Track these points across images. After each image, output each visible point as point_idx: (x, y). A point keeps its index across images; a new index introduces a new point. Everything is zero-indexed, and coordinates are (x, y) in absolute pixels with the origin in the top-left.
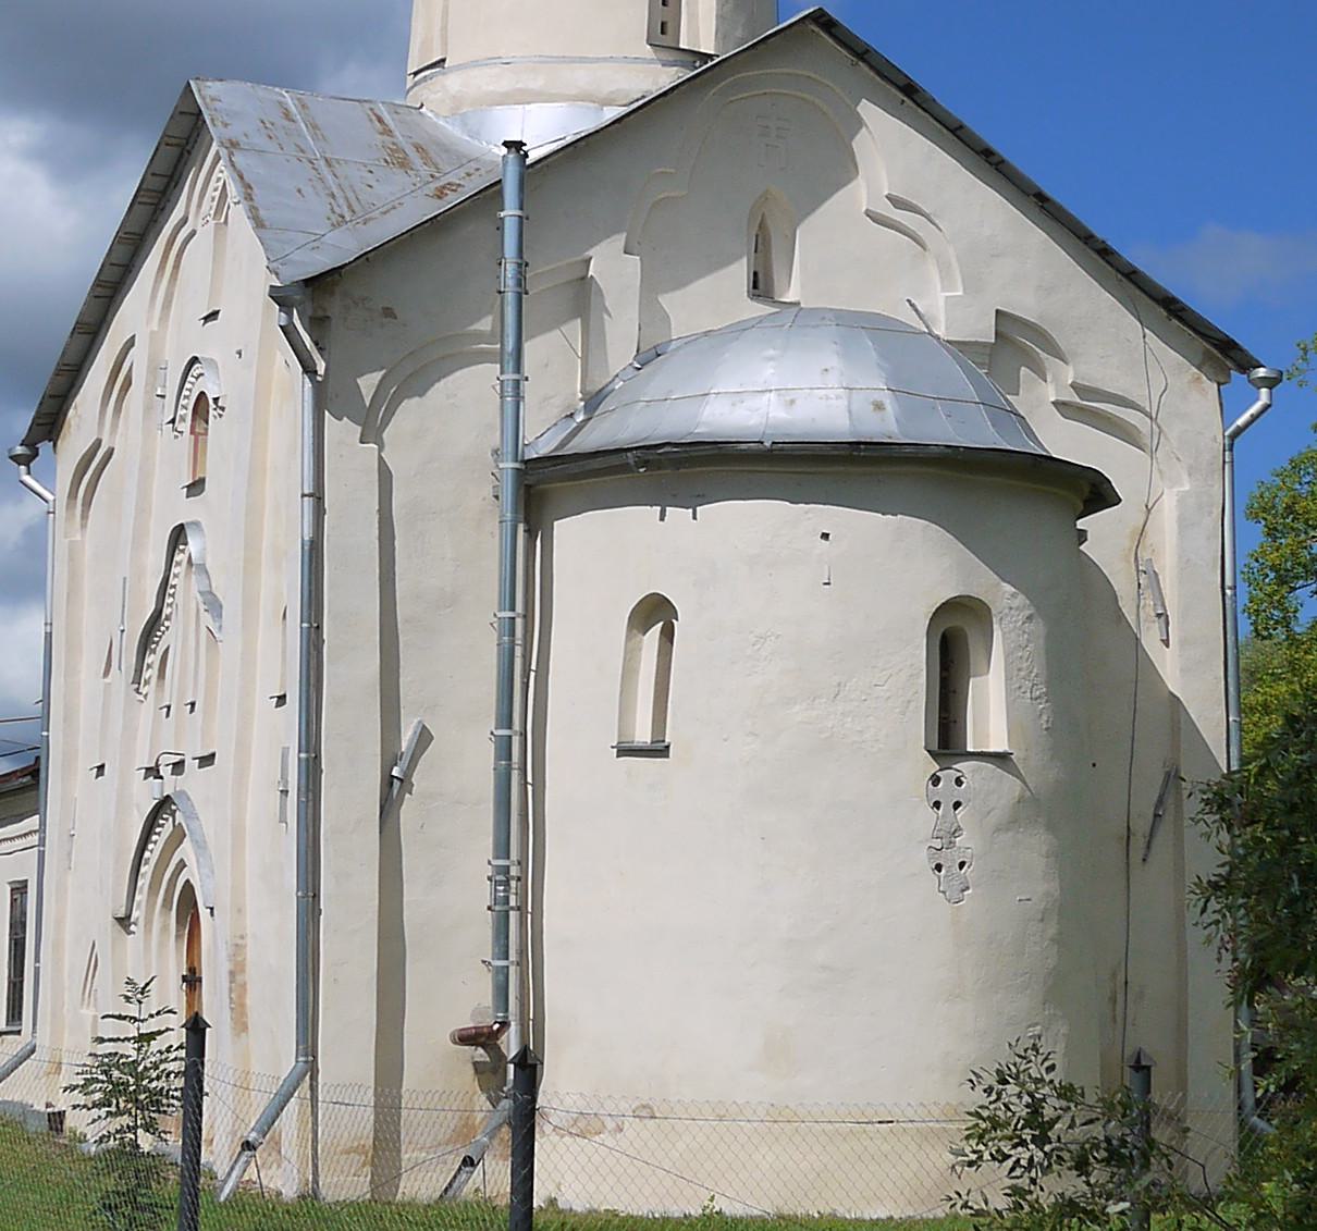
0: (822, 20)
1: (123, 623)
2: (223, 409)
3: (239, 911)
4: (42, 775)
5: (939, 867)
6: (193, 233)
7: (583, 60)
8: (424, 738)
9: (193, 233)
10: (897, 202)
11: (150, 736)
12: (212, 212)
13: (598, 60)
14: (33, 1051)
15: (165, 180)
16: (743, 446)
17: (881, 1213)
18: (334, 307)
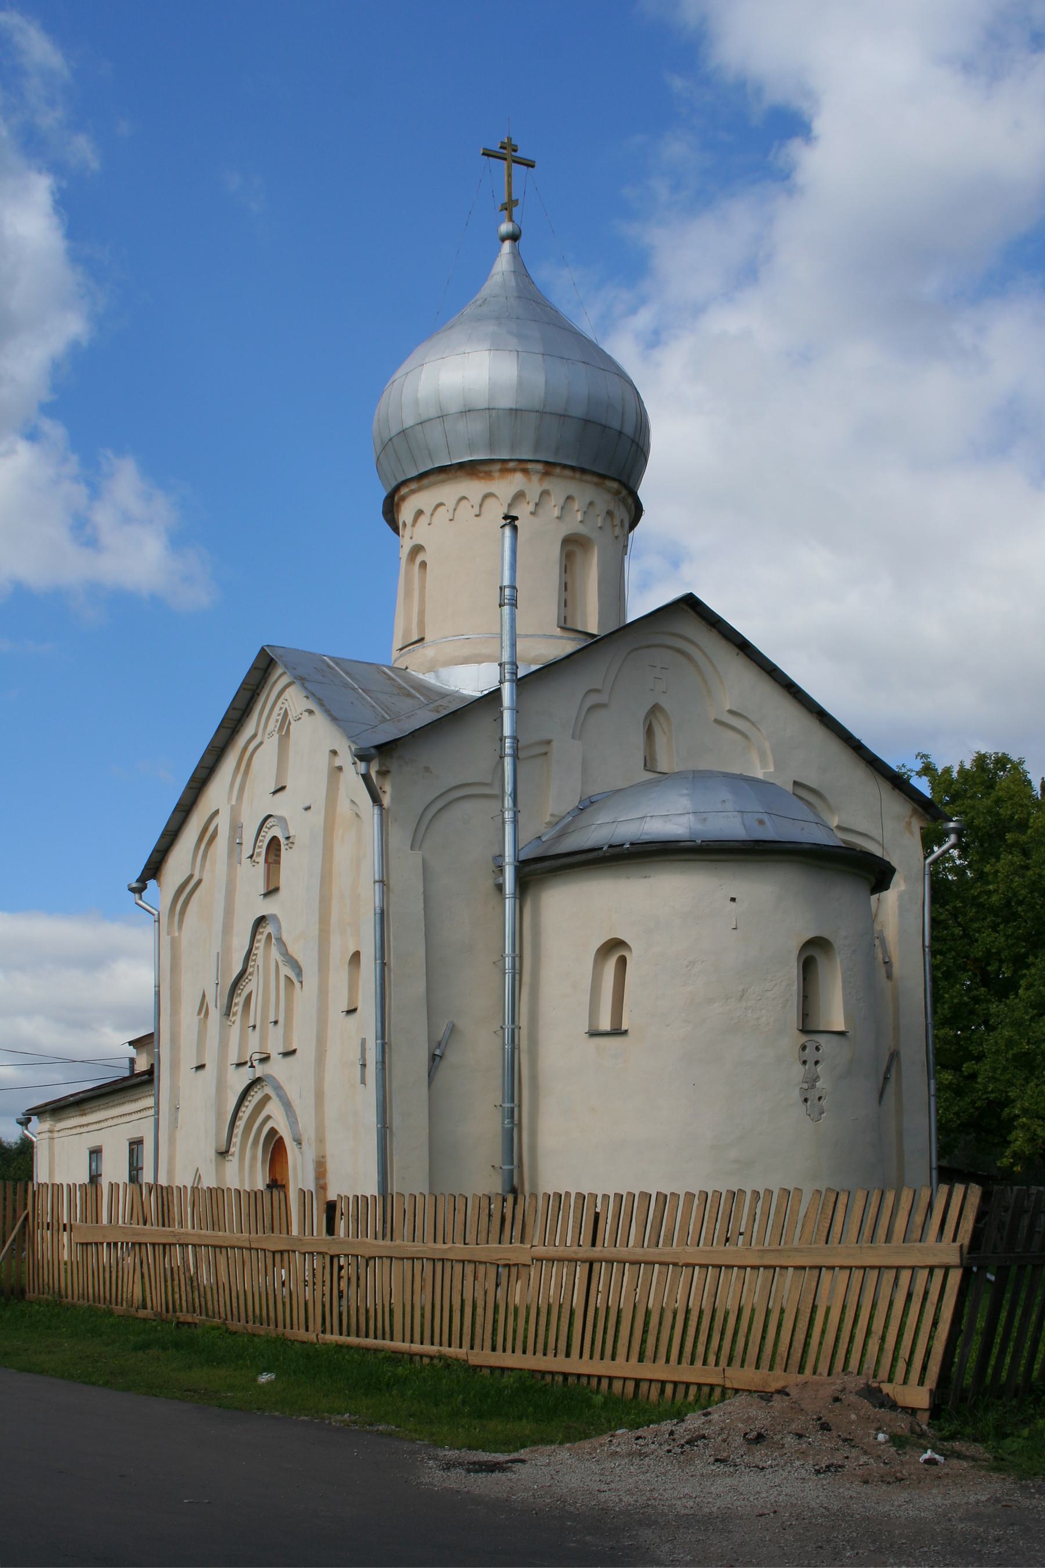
0: (690, 604)
2: (293, 843)
3: (321, 1141)
5: (806, 1100)
6: (261, 743)
9: (261, 743)
11: (239, 1041)
16: (682, 844)
18: (394, 766)
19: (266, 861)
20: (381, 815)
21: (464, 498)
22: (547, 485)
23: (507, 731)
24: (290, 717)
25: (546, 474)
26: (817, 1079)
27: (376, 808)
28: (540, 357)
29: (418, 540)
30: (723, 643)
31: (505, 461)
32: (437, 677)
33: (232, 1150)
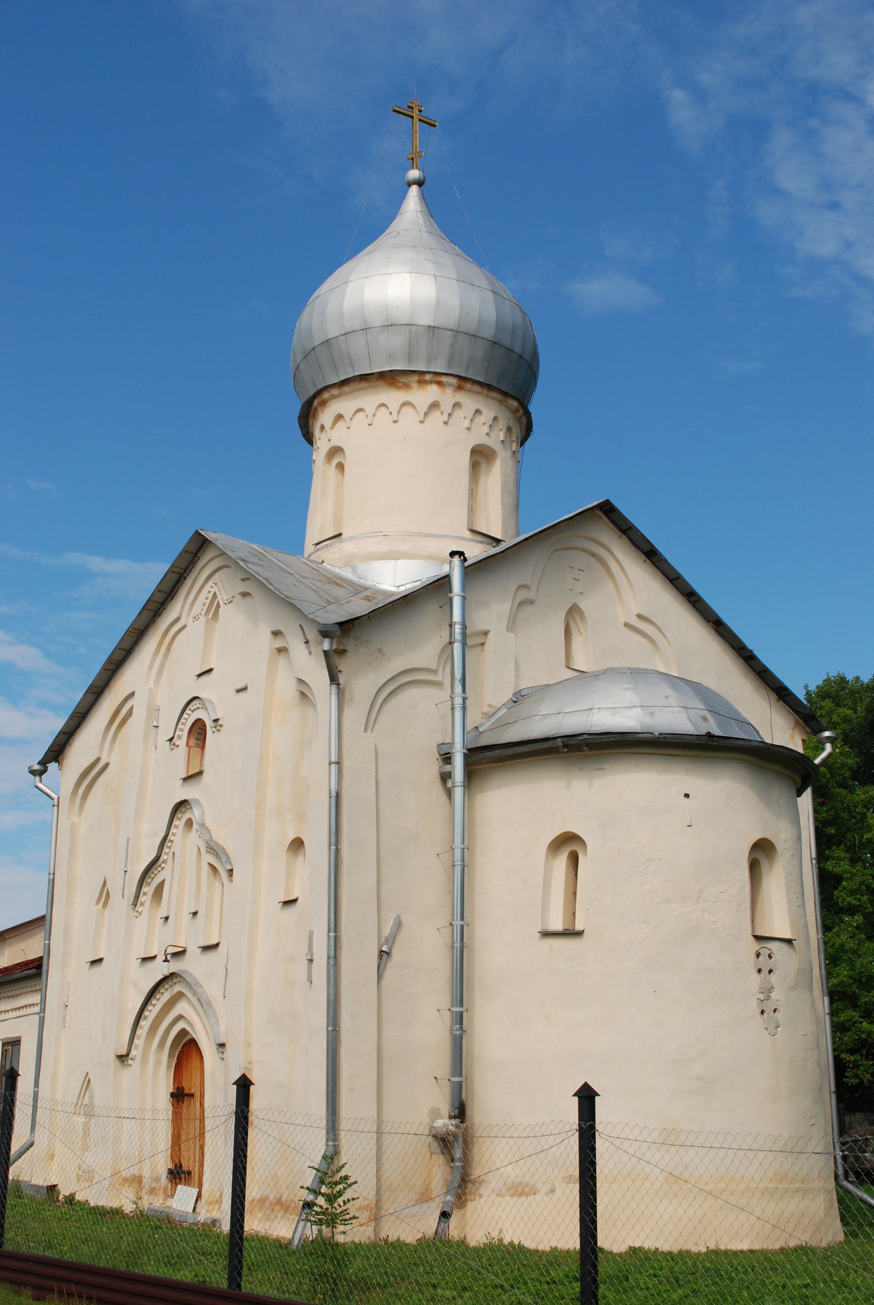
0: (607, 509)
1: (126, 866)
2: (221, 726)
3: (249, 1045)
4: (44, 968)
5: (762, 1012)
6: (185, 627)
7: (432, 536)
8: (398, 925)
9: (185, 627)
10: (640, 617)
11: (149, 934)
12: (203, 613)
13: (441, 536)
14: (32, 1145)
15: (166, 595)
17: (744, 1246)
19: (187, 744)
20: (338, 694)
21: (360, 410)
22: (460, 397)
23: (457, 616)
24: (219, 598)
25: (459, 388)
26: (771, 989)
27: (334, 687)
28: (455, 282)
29: (335, 443)
30: (633, 548)
31: (422, 373)
32: (354, 571)
33: (134, 1052)
